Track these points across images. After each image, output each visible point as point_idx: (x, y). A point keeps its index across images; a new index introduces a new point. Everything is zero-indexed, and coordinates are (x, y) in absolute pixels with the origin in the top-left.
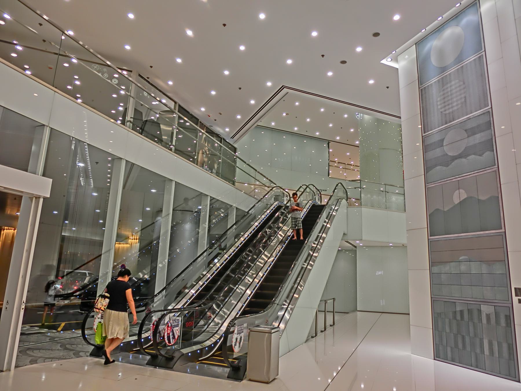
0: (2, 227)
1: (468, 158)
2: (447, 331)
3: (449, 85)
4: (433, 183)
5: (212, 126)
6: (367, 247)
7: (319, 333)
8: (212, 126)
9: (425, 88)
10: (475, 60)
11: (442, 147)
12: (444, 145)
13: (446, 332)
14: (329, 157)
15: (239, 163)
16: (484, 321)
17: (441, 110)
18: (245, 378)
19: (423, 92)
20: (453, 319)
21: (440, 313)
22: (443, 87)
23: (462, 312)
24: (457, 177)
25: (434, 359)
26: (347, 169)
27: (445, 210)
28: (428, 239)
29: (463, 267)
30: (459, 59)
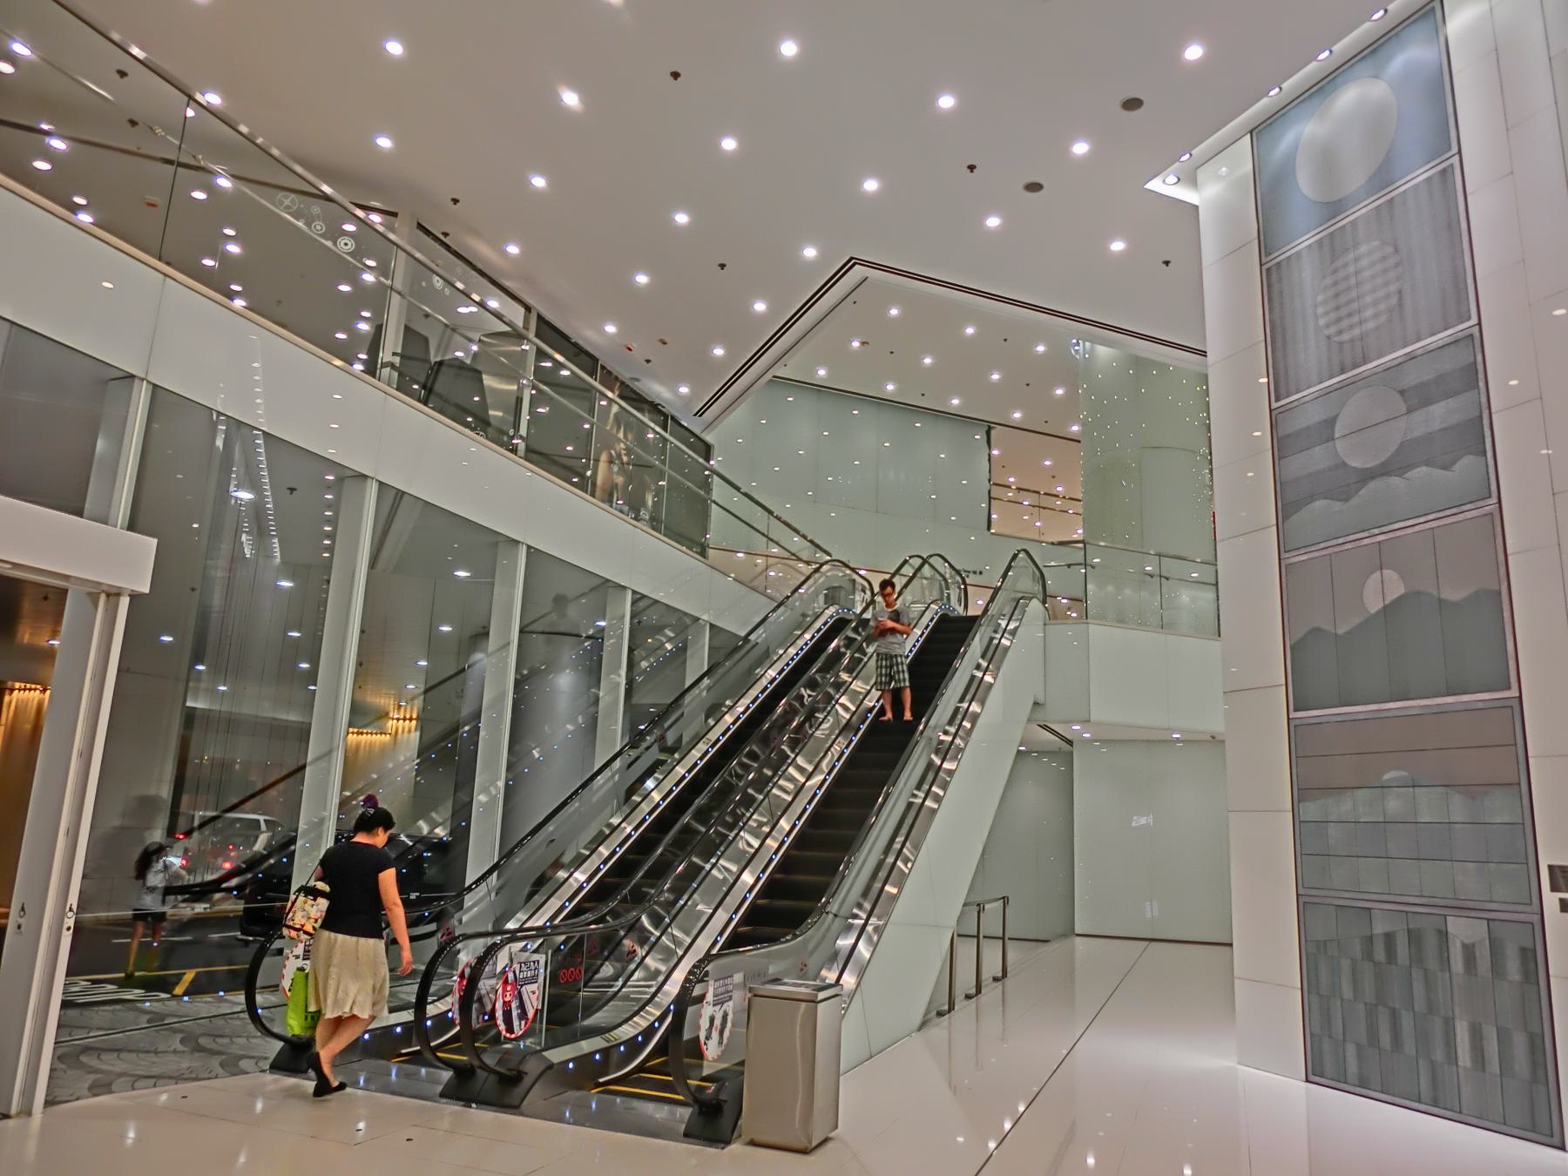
0: (6, 682)
1: (1408, 475)
2: (1345, 997)
3: (1351, 256)
4: (1302, 551)
5: (638, 380)
6: (1105, 742)
7: (960, 1002)
8: (638, 380)
9: (1278, 264)
10: (1428, 180)
11: (1330, 443)
12: (1337, 435)
13: (1342, 1000)
14: (990, 472)
15: (719, 490)
16: (1458, 964)
17: (1327, 332)
18: (736, 1138)
19: (1273, 278)
20: (1363, 960)
21: (1325, 942)
22: (1333, 262)
23: (1389, 938)
24: (1376, 531)
25: (1307, 1081)
26: (1044, 508)
27: (1340, 631)
28: (1288, 719)
29: (1394, 805)
30: (1382, 178)
